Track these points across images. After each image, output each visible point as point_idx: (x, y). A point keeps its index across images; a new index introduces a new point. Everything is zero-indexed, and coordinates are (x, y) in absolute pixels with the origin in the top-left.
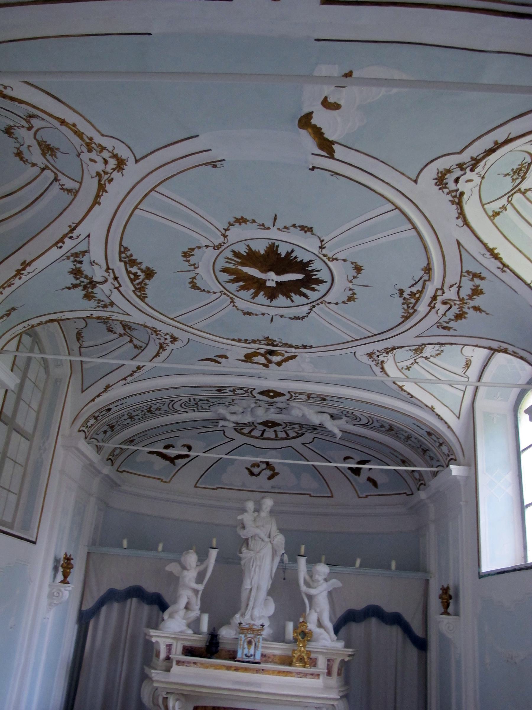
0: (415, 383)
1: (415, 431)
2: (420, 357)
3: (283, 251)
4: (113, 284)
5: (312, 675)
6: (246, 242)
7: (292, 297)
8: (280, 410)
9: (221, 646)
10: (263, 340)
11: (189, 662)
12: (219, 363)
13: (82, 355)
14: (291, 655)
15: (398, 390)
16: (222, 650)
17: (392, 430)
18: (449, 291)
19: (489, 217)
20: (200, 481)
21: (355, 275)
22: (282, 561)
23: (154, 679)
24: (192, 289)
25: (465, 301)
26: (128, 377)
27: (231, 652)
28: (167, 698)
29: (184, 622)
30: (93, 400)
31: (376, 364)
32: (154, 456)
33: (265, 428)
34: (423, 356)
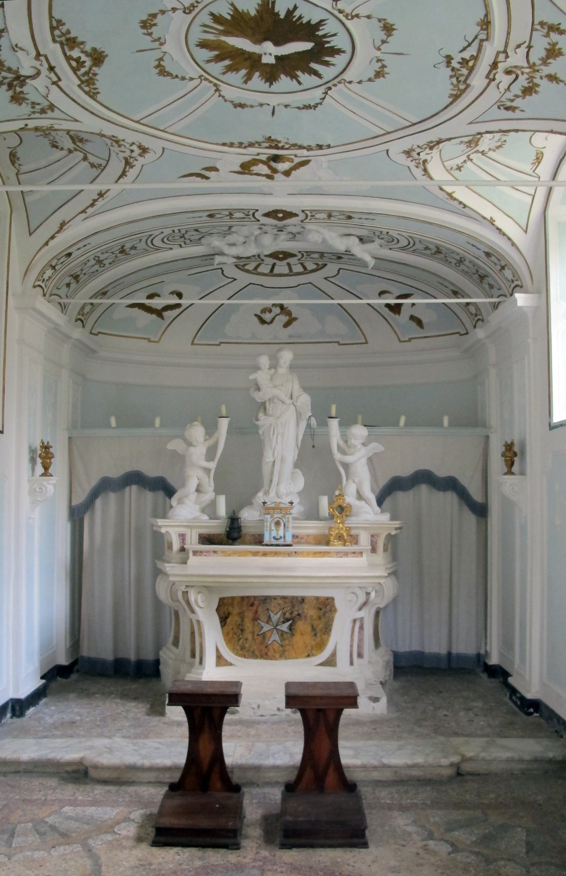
0: (467, 187)
1: (468, 251)
2: (475, 152)
4: (50, 78)
5: (354, 553)
7: (299, 77)
8: (294, 236)
9: (244, 531)
10: (263, 142)
11: (207, 552)
12: (207, 178)
13: (21, 183)
14: (328, 534)
15: (447, 199)
16: (246, 534)
17: (440, 253)
18: (515, 54)
20: (197, 337)
21: (384, 38)
22: (309, 425)
23: (169, 573)
24: (159, 76)
25: (536, 68)
26: (87, 208)
27: (257, 536)
28: (187, 592)
29: (197, 507)
30: (47, 244)
31: (416, 164)
32: (136, 309)
33: (275, 261)
34: (478, 151)
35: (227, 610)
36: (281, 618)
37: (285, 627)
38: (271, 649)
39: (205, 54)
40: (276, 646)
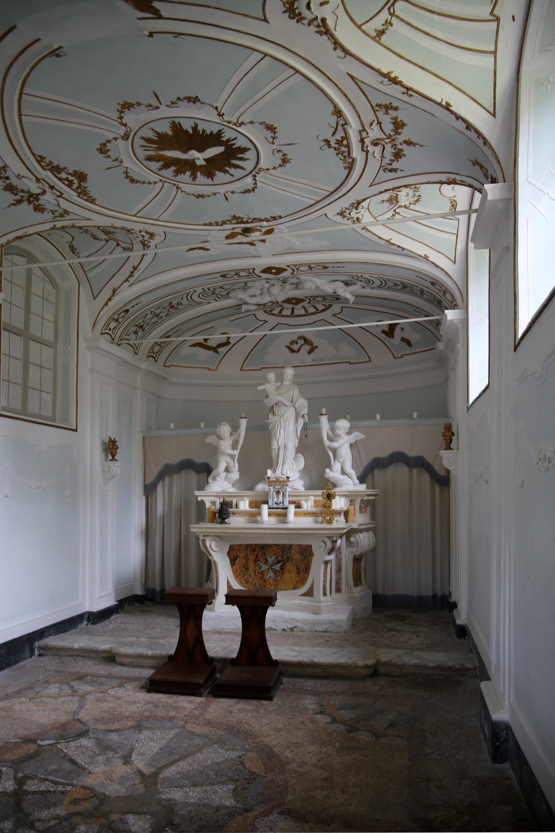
3: (187, 126)
4: (54, 193)
6: (149, 126)
17: (407, 287)
19: (373, 38)
26: (128, 278)
28: (205, 540)
30: (106, 304)
33: (293, 306)
34: (401, 206)
35: (236, 554)
36: (275, 560)
37: (277, 567)
38: (268, 583)
39: (155, 165)
40: (271, 581)
